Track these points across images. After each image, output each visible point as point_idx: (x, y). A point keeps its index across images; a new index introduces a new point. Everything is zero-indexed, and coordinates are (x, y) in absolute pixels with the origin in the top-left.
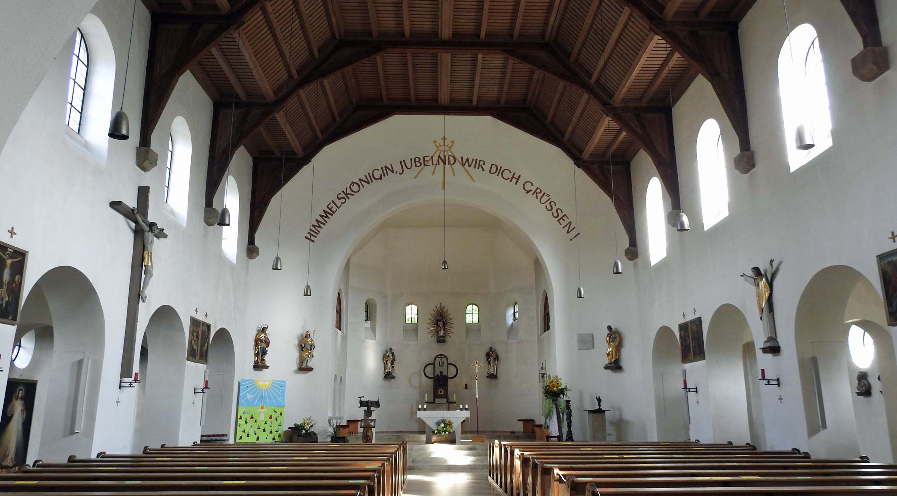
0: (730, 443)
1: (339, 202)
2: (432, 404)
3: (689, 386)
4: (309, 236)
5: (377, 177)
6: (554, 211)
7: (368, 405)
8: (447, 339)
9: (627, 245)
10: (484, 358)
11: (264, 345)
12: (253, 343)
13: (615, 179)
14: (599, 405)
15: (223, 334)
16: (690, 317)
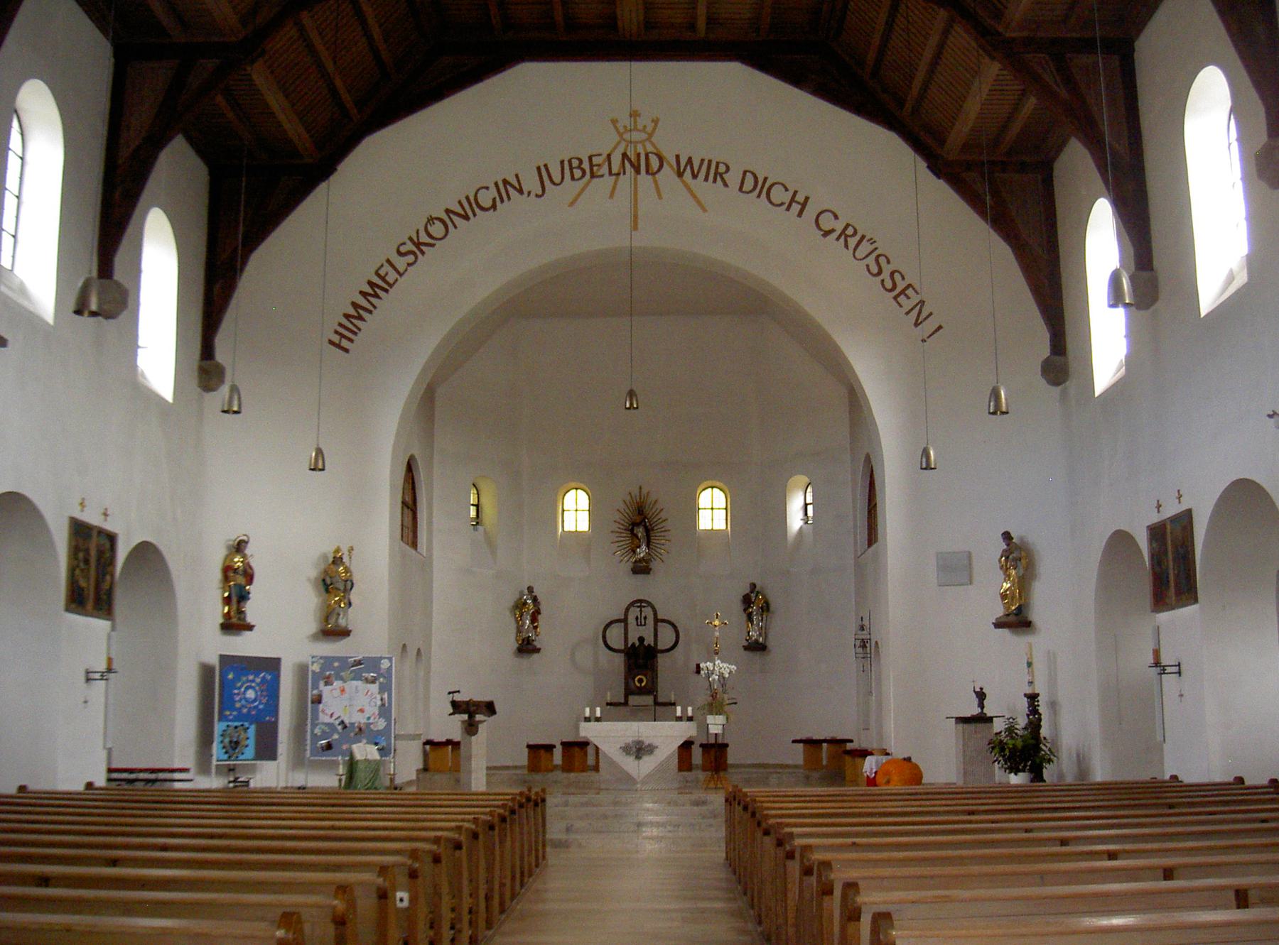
0: (1240, 780)
1: (401, 263)
2: (619, 707)
3: (1164, 662)
4: (336, 339)
5: (486, 203)
6: (886, 275)
7: (472, 711)
8: (655, 565)
9: (1046, 352)
10: (738, 606)
11: (241, 580)
12: (218, 575)
13: (1018, 203)
14: (981, 706)
15: (146, 553)
16: (1172, 509)
